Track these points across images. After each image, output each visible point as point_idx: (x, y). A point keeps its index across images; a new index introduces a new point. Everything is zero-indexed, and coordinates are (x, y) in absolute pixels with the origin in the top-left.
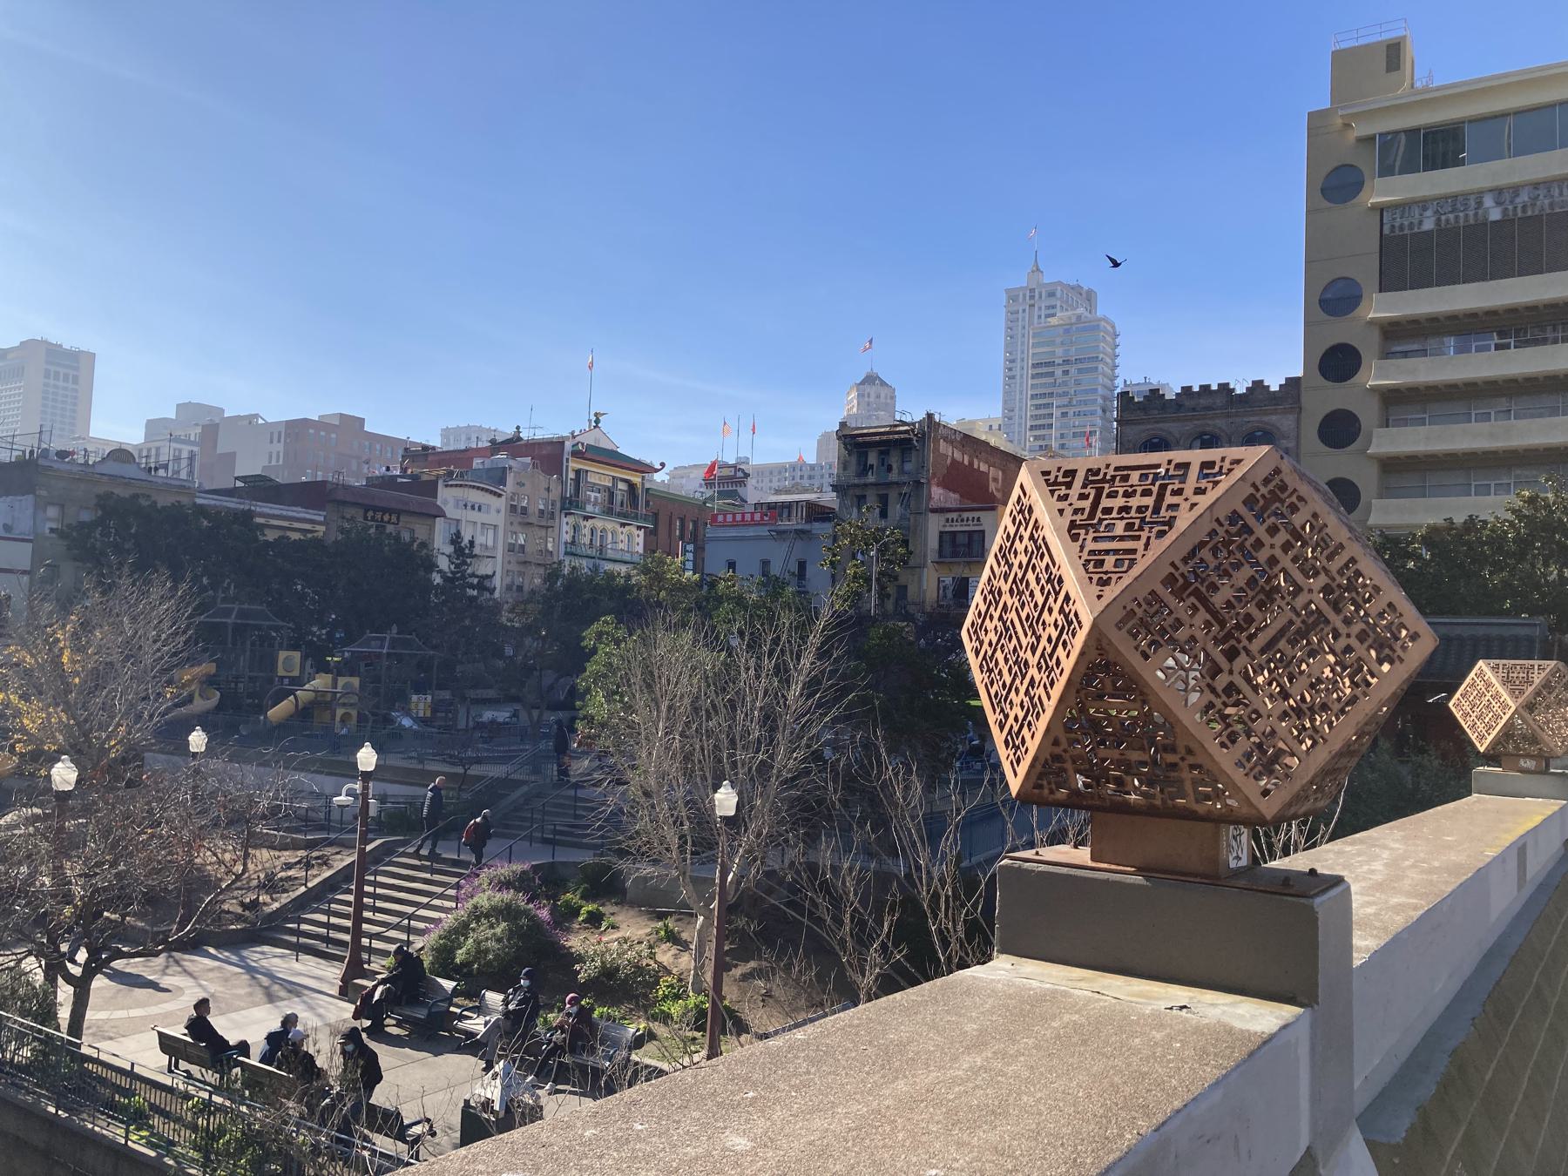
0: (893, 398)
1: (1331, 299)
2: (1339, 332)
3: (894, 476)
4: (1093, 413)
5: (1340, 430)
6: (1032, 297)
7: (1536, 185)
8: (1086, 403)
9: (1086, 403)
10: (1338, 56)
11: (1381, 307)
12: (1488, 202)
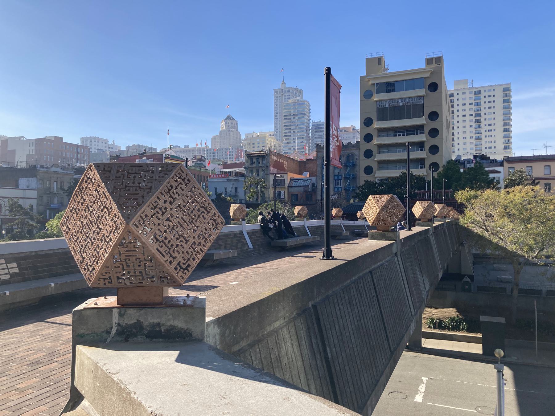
0: (237, 124)
1: (367, 122)
2: (369, 130)
3: (260, 165)
4: (303, 131)
5: (368, 154)
6: (282, 92)
7: (409, 98)
8: (301, 128)
9: (301, 128)
10: (369, 61)
11: (377, 125)
12: (400, 101)
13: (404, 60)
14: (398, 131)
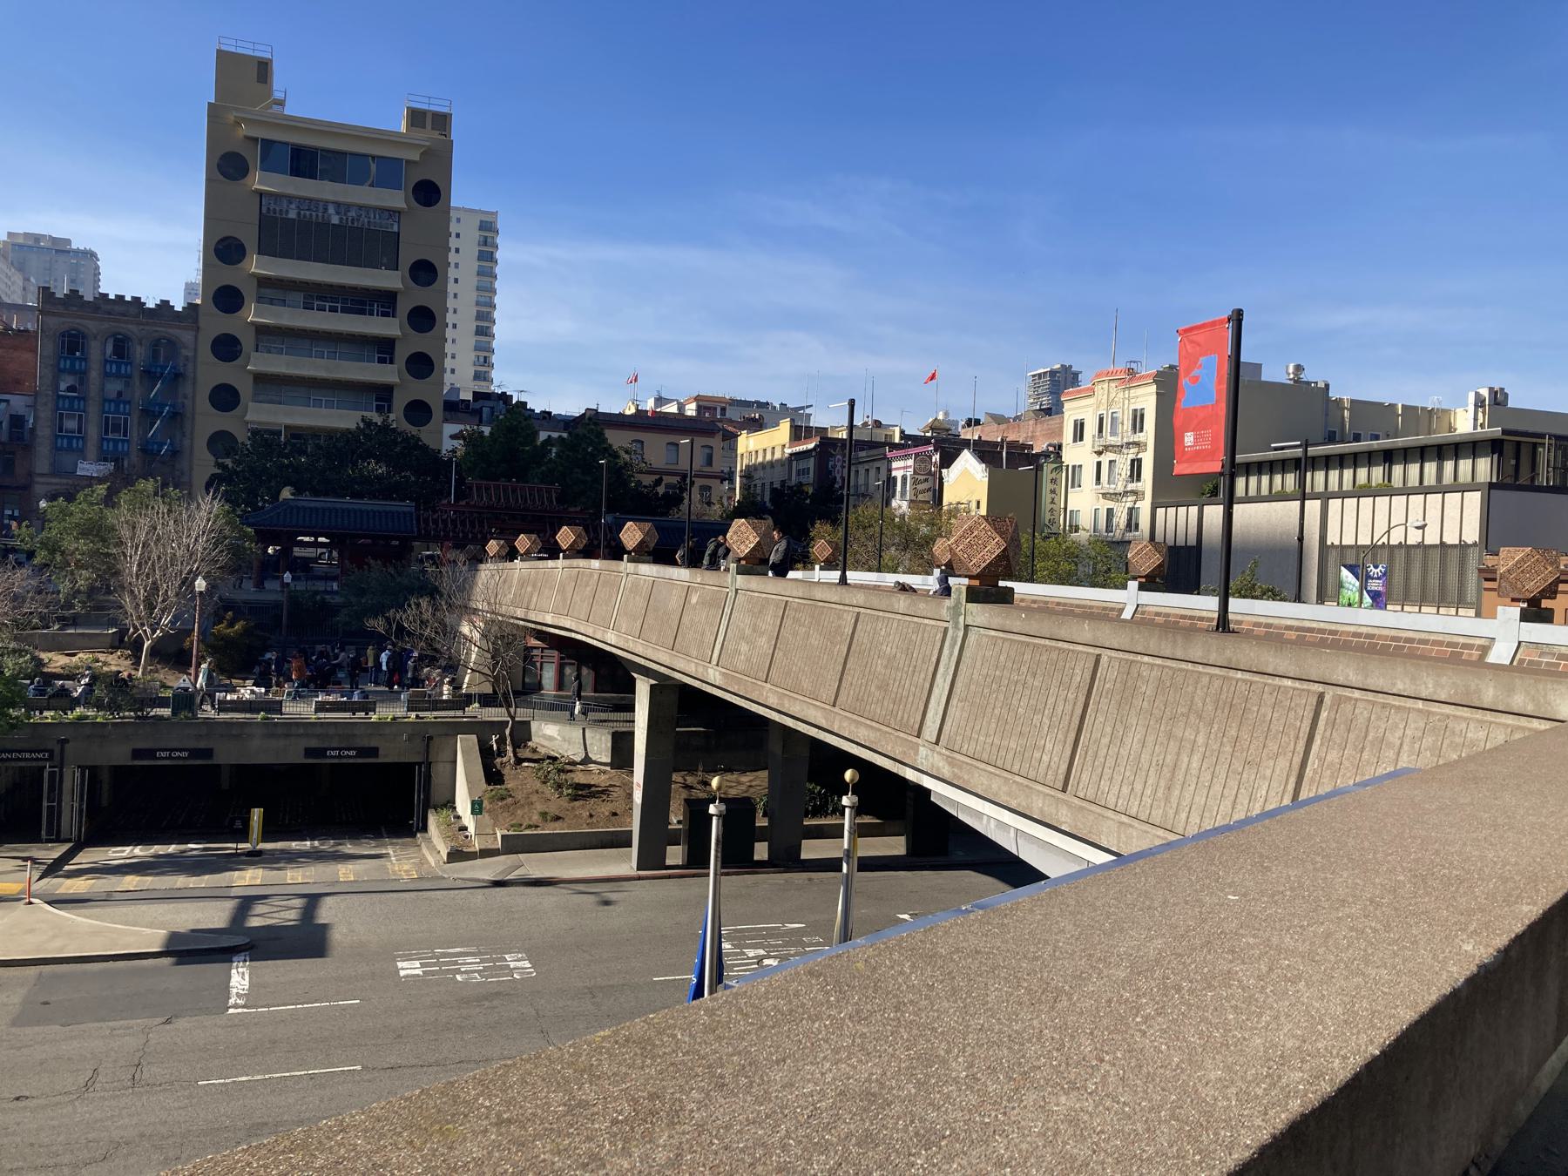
1: (223, 249)
7: (360, 207)
12: (331, 210)
13: (340, 89)
14: (317, 295)
